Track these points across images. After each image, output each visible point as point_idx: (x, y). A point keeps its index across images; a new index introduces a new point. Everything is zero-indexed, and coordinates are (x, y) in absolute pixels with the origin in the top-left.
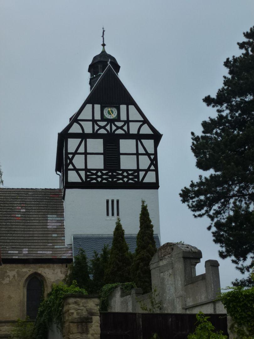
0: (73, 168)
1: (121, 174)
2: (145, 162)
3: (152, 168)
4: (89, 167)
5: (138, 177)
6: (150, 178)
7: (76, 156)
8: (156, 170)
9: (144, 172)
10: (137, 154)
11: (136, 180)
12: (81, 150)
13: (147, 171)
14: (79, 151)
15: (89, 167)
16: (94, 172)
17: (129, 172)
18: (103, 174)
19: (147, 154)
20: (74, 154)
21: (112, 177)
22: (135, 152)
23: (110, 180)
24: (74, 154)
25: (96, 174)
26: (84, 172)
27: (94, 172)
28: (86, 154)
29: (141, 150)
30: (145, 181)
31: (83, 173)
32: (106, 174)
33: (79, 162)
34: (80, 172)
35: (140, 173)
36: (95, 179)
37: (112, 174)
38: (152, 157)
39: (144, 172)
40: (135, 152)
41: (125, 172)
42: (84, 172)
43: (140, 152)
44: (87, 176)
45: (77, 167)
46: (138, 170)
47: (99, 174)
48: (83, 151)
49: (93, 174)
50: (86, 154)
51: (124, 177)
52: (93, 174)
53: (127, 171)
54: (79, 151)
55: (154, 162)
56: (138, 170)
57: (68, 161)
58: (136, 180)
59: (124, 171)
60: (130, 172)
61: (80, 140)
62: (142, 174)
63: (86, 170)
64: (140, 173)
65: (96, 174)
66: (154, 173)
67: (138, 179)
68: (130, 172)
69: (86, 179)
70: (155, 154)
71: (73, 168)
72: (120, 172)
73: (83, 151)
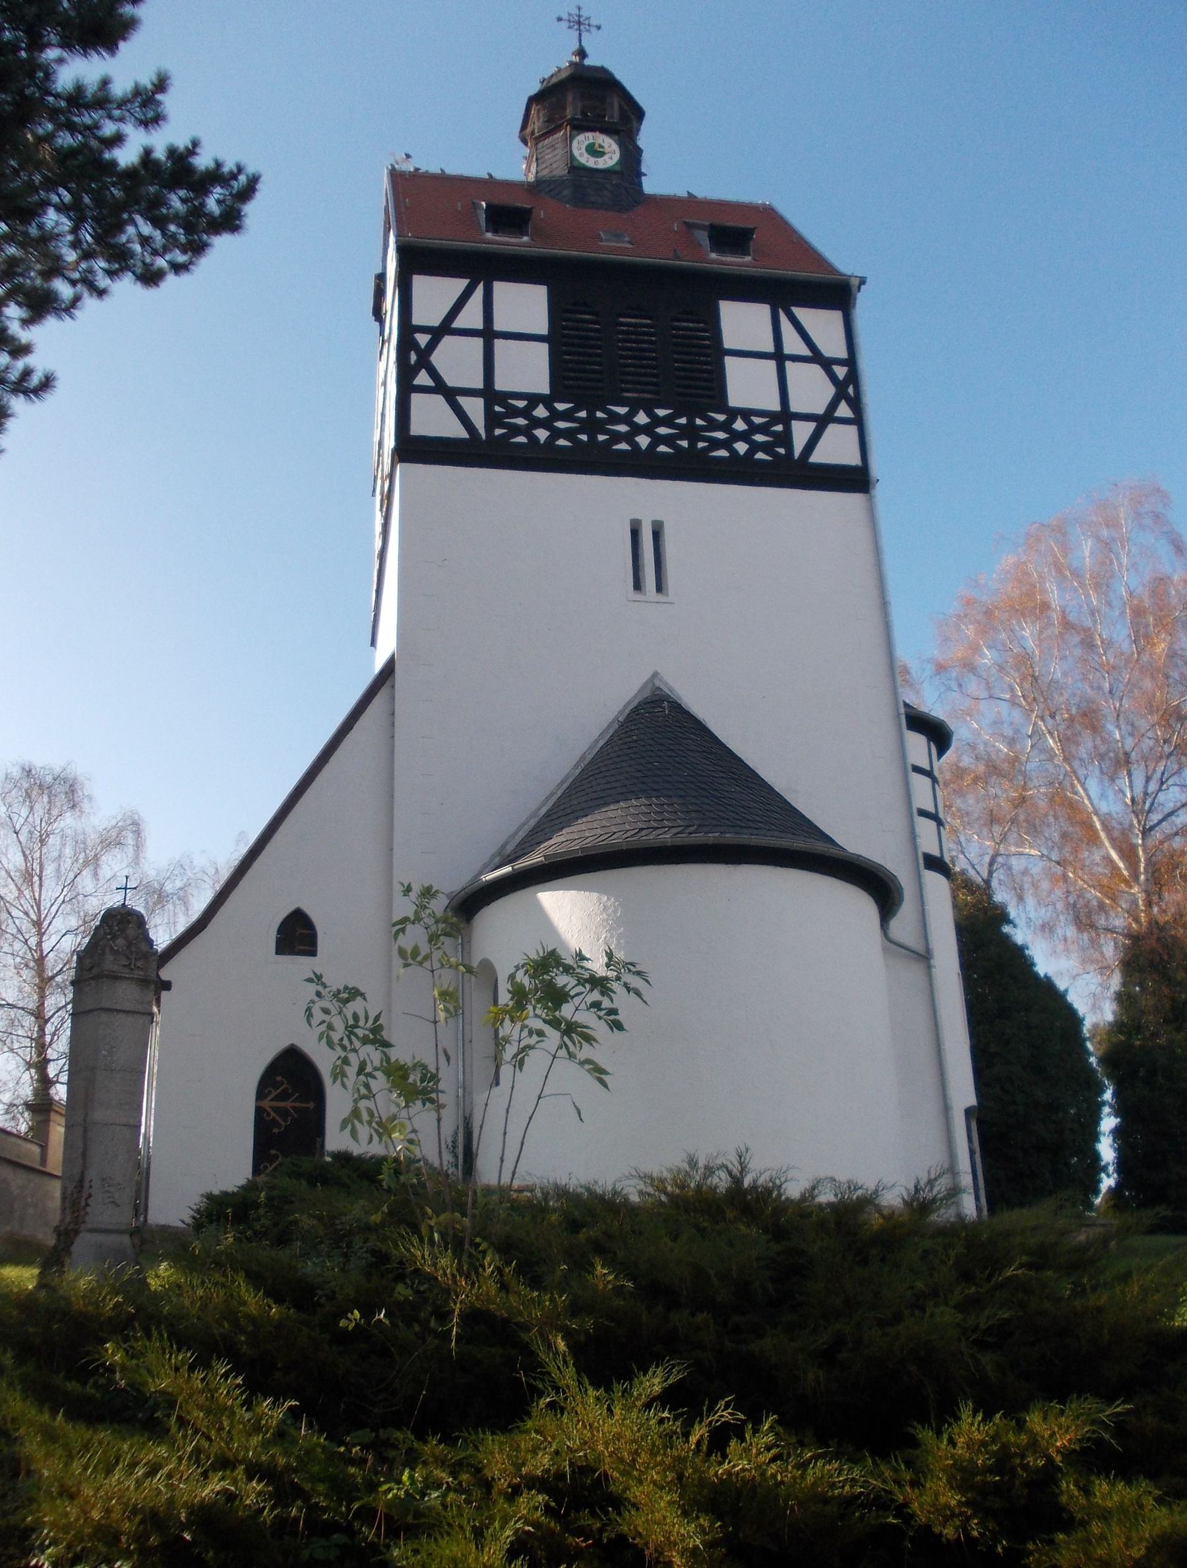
0: (430, 383)
1: (726, 426)
2: (811, 390)
3: (844, 410)
4: (500, 385)
5: (786, 439)
6: (839, 447)
7: (447, 341)
8: (858, 420)
9: (811, 426)
10: (779, 357)
11: (782, 451)
12: (472, 316)
13: (823, 421)
14: (458, 323)
15: (500, 385)
16: (521, 404)
17: (556, 405)
18: (556, 415)
19: (816, 357)
20: (439, 332)
21: (691, 432)
22: (499, 344)
23: (584, 437)
24: (439, 332)
25: (526, 413)
26: (480, 402)
27: (521, 404)
28: (488, 334)
29: (793, 344)
30: (816, 458)
31: (475, 408)
32: (566, 416)
33: (458, 361)
34: (462, 400)
35: (796, 425)
36: (726, 445)
37: (591, 414)
38: (841, 372)
39: (811, 426)
40: (499, 344)
41: (541, 406)
42: (480, 402)
43: (788, 350)
44: (492, 420)
45: (451, 381)
46: (786, 415)
47: (541, 412)
48: (479, 324)
49: (517, 413)
50: (488, 334)
51: (737, 436)
52: (517, 413)
53: (746, 414)
54: (458, 323)
55: (848, 387)
56: (786, 415)
57: (413, 357)
58: (782, 451)
59: (734, 413)
60: (757, 420)
61: (462, 283)
62: (801, 432)
63: (489, 393)
64: (796, 425)
65: (526, 413)
66: (852, 430)
67: (789, 445)
68: (757, 420)
69: (489, 427)
70: (851, 362)
71: (430, 383)
72: (721, 418)
73: (479, 324)
